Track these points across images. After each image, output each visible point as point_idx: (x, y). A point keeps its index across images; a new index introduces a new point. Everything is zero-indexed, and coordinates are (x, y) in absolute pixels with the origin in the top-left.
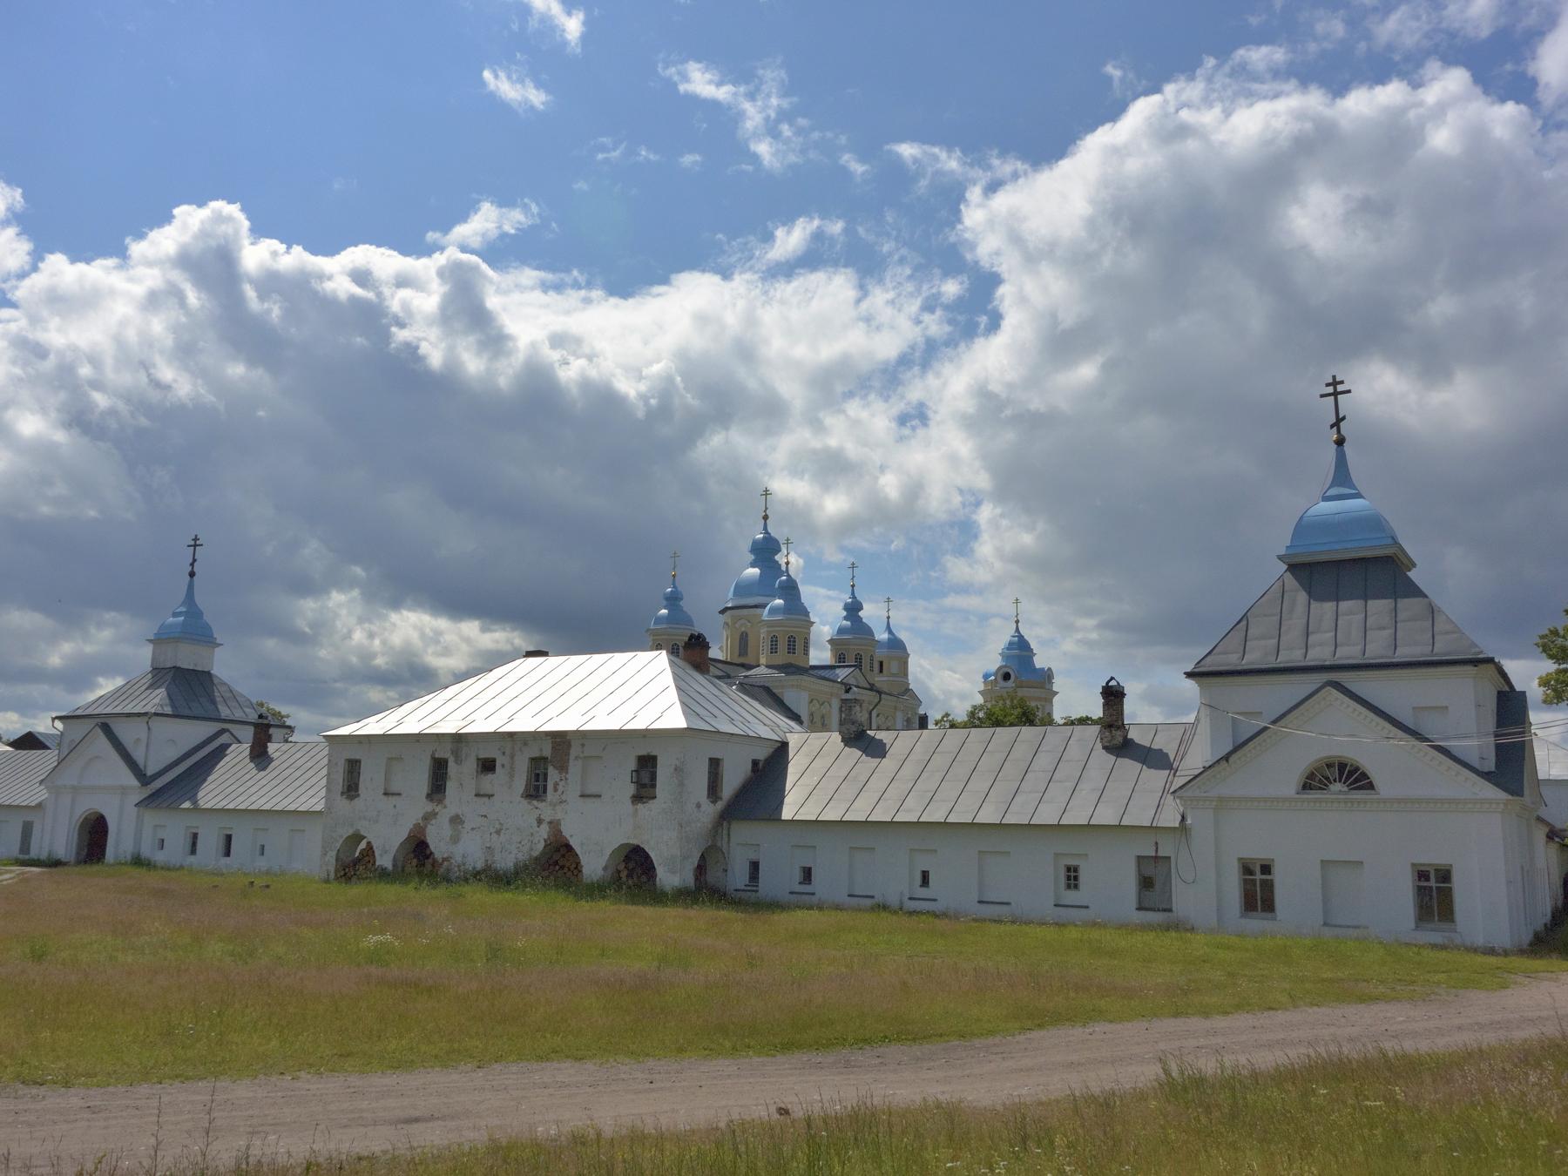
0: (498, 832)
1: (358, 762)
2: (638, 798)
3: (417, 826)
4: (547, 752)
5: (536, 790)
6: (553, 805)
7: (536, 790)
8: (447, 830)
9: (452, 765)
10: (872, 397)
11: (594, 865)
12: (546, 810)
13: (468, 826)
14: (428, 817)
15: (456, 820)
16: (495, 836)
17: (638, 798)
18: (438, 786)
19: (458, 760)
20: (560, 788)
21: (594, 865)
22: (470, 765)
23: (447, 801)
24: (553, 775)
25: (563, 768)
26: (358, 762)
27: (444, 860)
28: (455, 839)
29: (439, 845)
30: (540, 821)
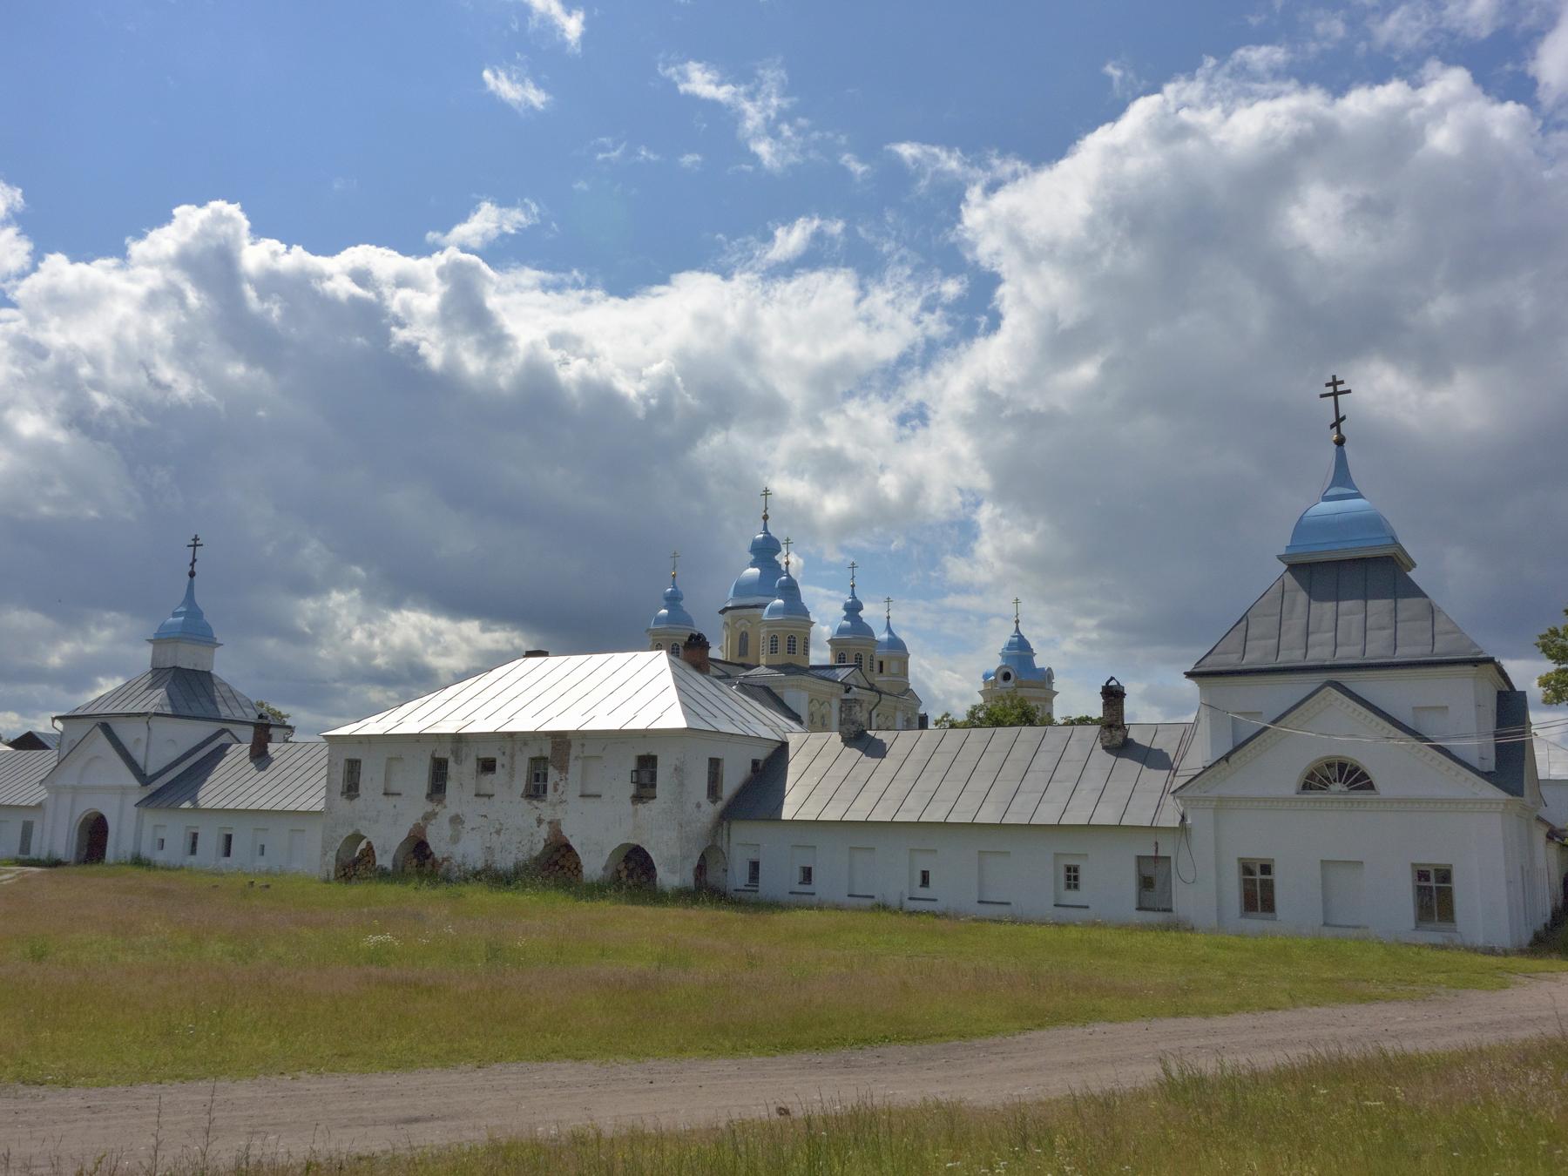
0: (498, 832)
1: (358, 762)
2: (638, 798)
3: (417, 826)
4: (547, 752)
5: (536, 790)
6: (553, 805)
7: (536, 790)
8: (447, 830)
9: (452, 765)
10: (872, 397)
11: (594, 865)
12: (546, 810)
13: (468, 826)
14: (428, 817)
15: (456, 820)
16: (495, 836)
17: (638, 798)
18: (438, 786)
19: (458, 760)
20: (560, 788)
21: (594, 865)
22: (470, 765)
23: (447, 801)
24: (553, 775)
25: (563, 768)
26: (358, 762)
27: (444, 860)
28: (455, 839)
29: (439, 845)
30: (540, 821)
